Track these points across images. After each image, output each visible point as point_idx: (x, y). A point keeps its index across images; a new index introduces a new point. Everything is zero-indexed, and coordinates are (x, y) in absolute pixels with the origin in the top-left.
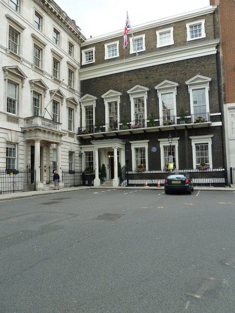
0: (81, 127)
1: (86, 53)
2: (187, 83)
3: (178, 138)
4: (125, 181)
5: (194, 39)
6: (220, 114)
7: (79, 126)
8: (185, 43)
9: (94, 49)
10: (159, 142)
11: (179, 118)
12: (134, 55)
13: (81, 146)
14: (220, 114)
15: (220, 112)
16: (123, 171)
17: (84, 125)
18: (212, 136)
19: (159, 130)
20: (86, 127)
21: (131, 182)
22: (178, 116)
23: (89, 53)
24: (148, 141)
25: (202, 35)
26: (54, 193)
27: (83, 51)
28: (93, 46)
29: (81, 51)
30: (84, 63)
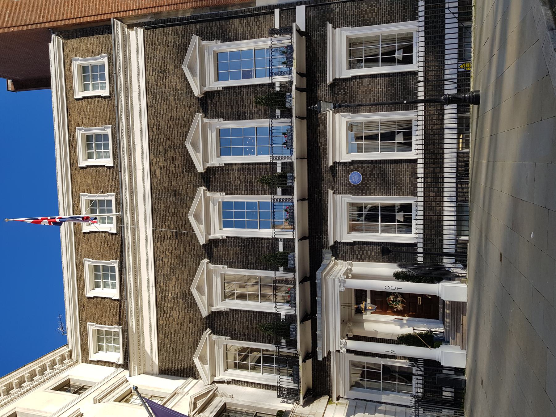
0: (278, 388)
1: (100, 349)
2: (197, 92)
3: (329, 26)
4: (447, 262)
5: (117, 281)
6: (277, 11)
7: (275, 393)
8: (115, 169)
9: (92, 327)
10: (336, 242)
11: (279, 190)
12: (120, 221)
13: (334, 396)
14: (277, 11)
15: (272, 13)
16: (409, 272)
17: (270, 378)
18: (330, 192)
19: (307, 241)
20: (279, 372)
21: (448, 244)
22: (274, 193)
23: (97, 277)
24: (329, 26)
25: (113, 265)
26: (475, 22)
27: (93, 357)
28: (86, 327)
29: (92, 362)
30: (117, 357)
